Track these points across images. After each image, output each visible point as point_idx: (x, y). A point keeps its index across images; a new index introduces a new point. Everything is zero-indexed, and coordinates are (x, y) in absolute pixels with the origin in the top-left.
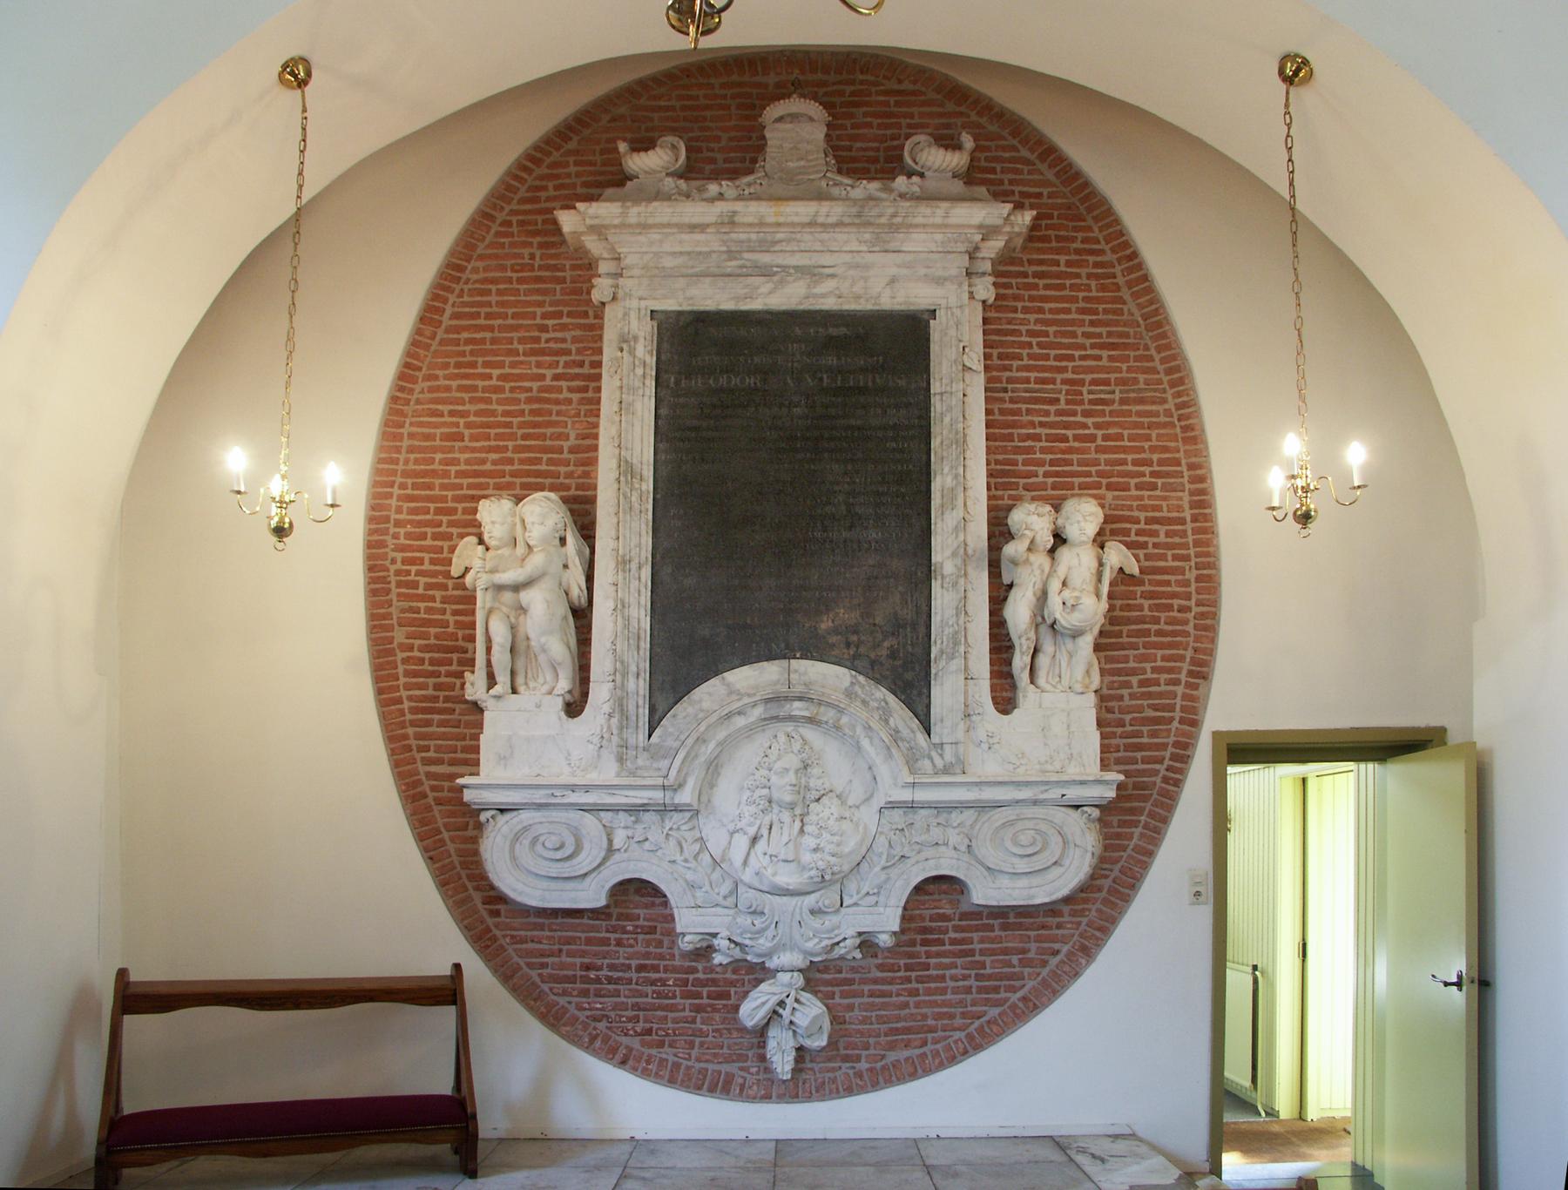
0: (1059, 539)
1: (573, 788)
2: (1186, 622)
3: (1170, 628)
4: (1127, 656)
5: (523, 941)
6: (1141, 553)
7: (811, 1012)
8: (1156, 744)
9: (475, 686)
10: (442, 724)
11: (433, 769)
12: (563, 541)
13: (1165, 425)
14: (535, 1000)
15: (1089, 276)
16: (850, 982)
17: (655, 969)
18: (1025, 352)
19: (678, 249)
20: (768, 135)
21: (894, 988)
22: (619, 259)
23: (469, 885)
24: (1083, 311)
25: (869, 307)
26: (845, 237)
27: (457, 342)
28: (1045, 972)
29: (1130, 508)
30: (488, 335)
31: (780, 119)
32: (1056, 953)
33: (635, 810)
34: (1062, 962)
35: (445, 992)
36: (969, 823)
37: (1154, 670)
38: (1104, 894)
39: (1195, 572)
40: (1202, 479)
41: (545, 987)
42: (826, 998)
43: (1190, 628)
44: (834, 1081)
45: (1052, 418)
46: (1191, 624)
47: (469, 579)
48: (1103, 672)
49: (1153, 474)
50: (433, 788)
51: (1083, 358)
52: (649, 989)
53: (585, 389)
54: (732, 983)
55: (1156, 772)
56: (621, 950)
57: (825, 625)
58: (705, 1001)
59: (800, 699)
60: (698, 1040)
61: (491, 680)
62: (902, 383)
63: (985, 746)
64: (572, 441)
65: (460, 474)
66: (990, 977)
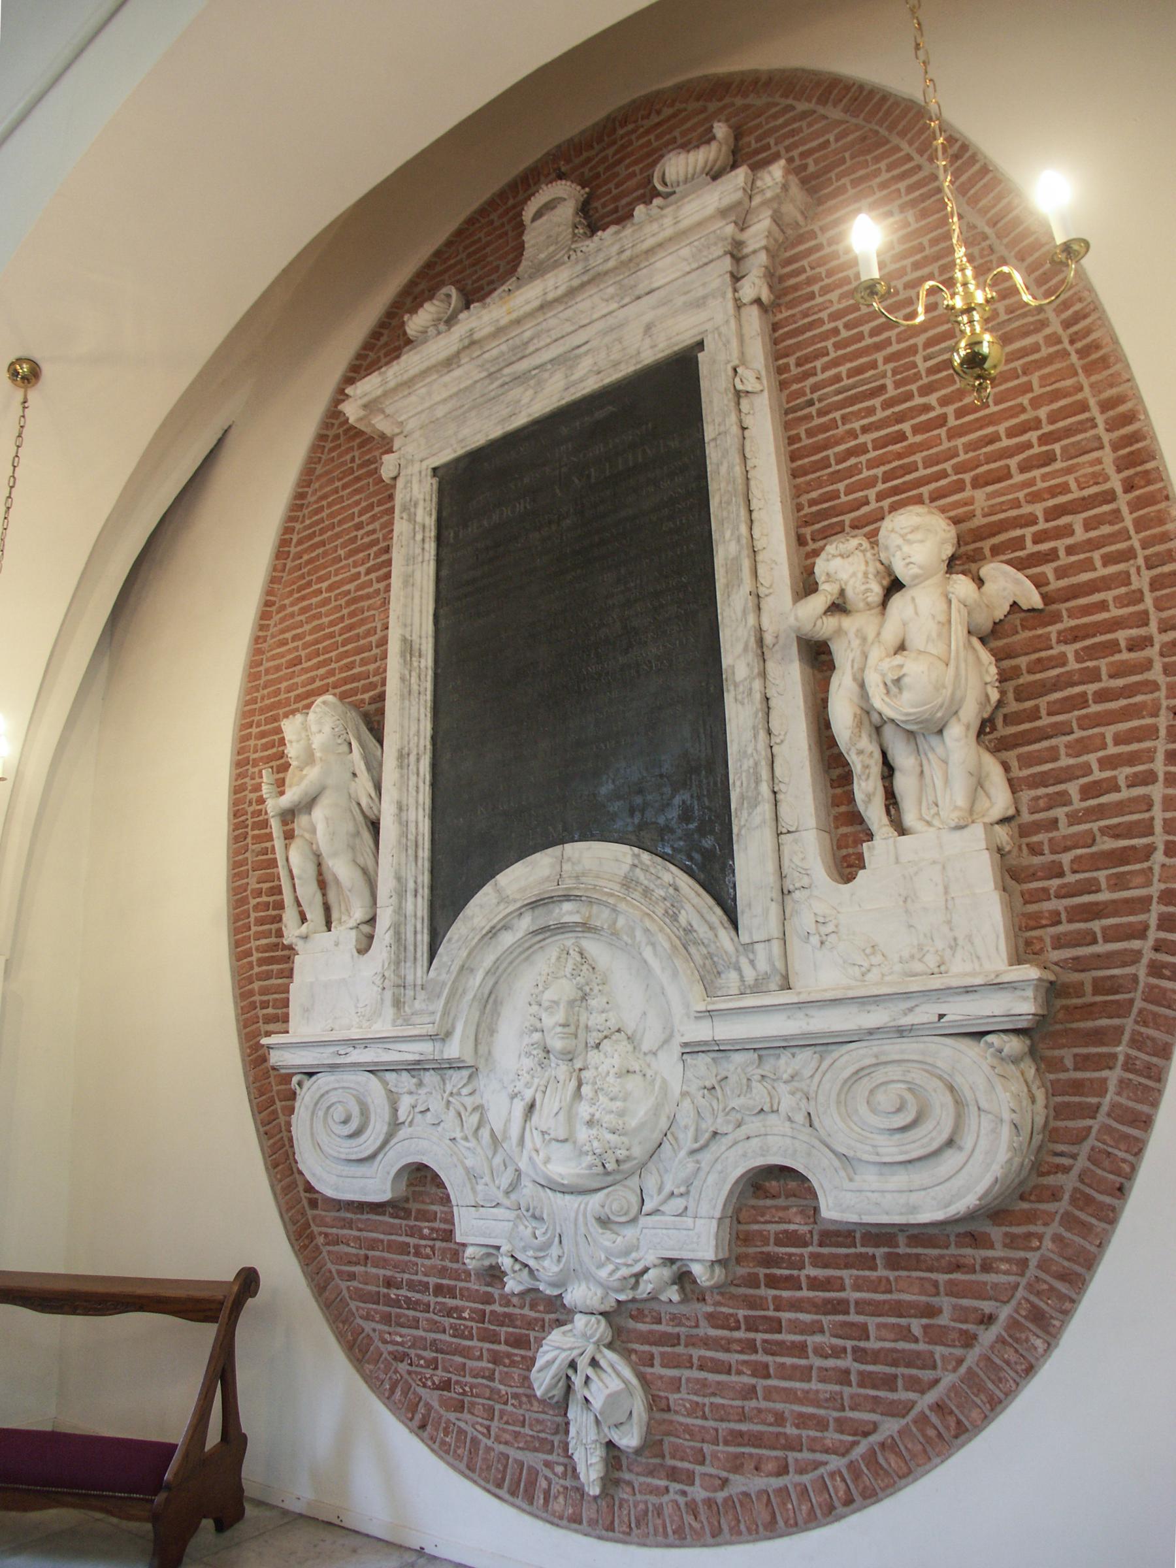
1: (353, 1043)
2: (1148, 665)
3: (1120, 682)
4: (1054, 749)
5: (337, 1241)
6: (1048, 569)
7: (612, 1384)
8: (1126, 901)
13: (1049, 360)
14: (344, 1322)
16: (674, 1340)
17: (451, 1292)
19: (445, 395)
21: (734, 1358)
26: (587, 304)
28: (972, 1357)
29: (1016, 504)
32: (988, 1320)
33: (415, 1068)
34: (1000, 1340)
35: (220, 1307)
36: (807, 1073)
37: (1105, 763)
38: (1064, 1205)
39: (1147, 575)
40: (1129, 418)
41: (353, 1305)
42: (641, 1364)
43: (1156, 674)
44: (659, 1511)
45: (880, 415)
46: (1158, 666)
48: (1014, 786)
49: (1043, 440)
54: (530, 1324)
55: (1136, 956)
56: (420, 1261)
57: (605, 789)
58: (503, 1348)
59: (567, 898)
62: (674, 444)
63: (815, 940)
66: (875, 1357)
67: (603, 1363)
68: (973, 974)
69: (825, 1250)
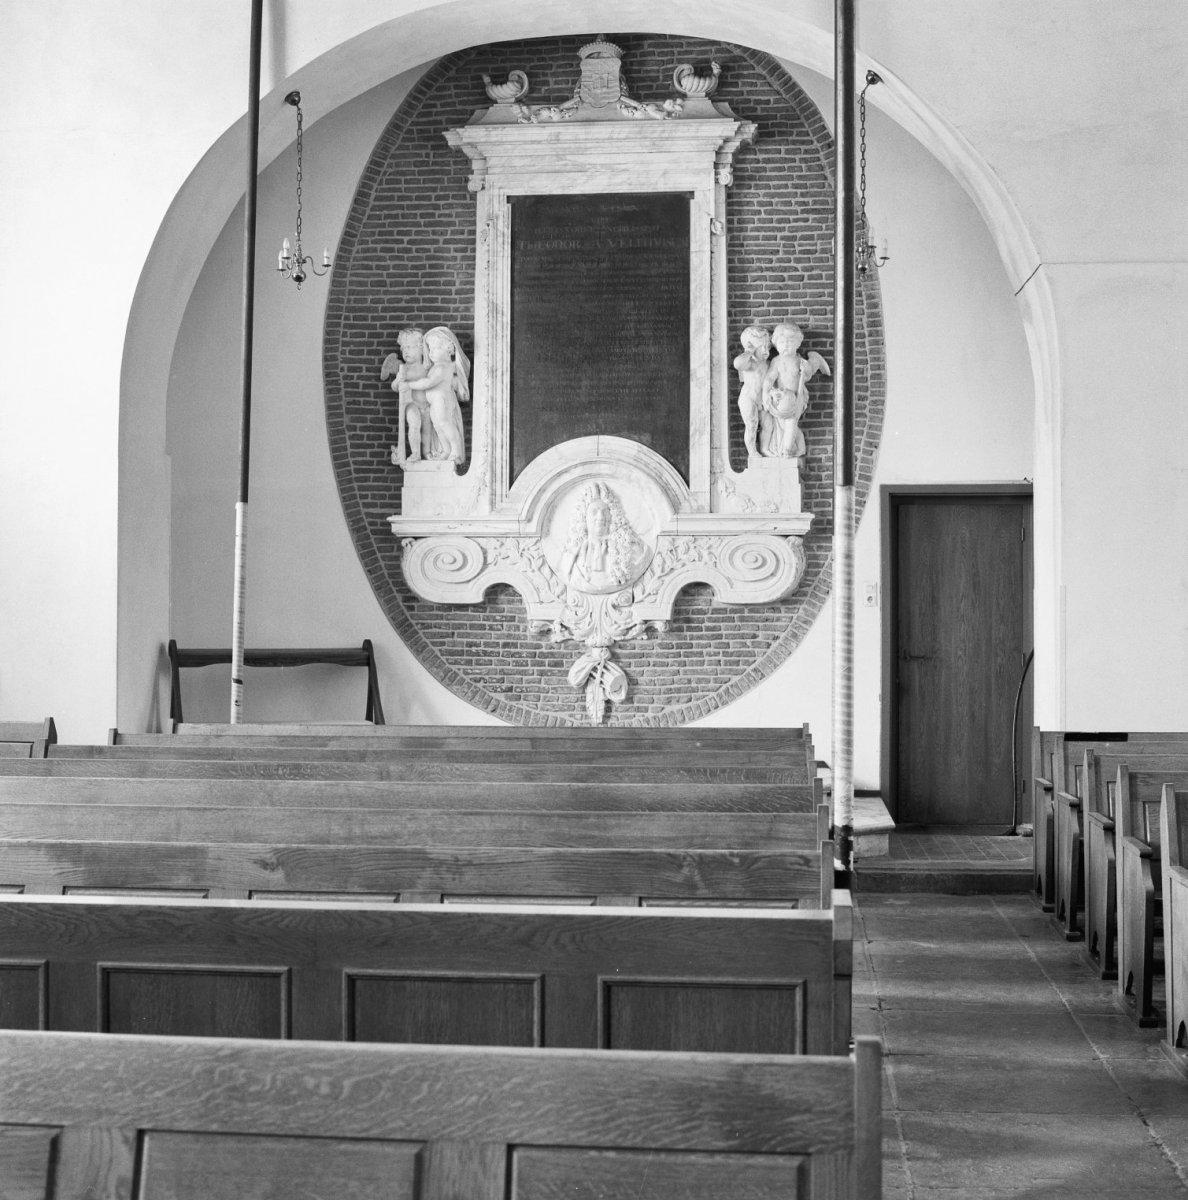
0: (774, 352)
5: (429, 627)
10: (376, 480)
11: (371, 510)
12: (453, 358)
15: (801, 160)
17: (515, 645)
18: (756, 217)
20: (583, 68)
21: (670, 660)
22: (485, 159)
23: (394, 589)
24: (796, 186)
25: (650, 190)
27: (379, 217)
28: (769, 651)
30: (400, 212)
31: (589, 57)
32: (776, 638)
35: (364, 657)
40: (876, 306)
41: (443, 658)
47: (394, 384)
50: (371, 524)
51: (796, 220)
52: (510, 660)
53: (464, 250)
54: (563, 656)
58: (547, 668)
59: (605, 462)
60: (542, 695)
61: (408, 453)
62: (672, 244)
64: (458, 286)
65: (385, 310)
66: (732, 654)
67: (609, 667)
68: (789, 514)
69: (714, 616)
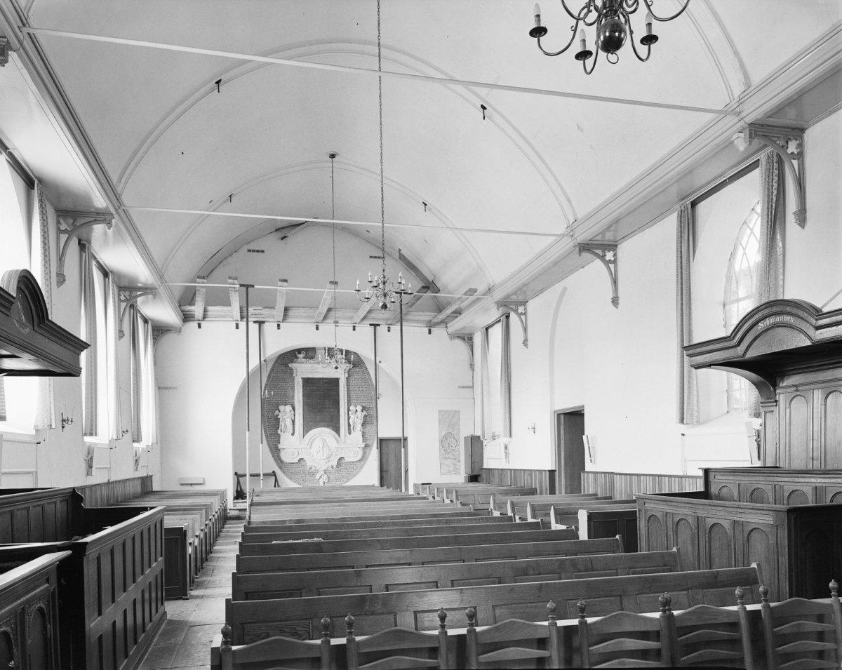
9: (279, 432)
35: (274, 474)
